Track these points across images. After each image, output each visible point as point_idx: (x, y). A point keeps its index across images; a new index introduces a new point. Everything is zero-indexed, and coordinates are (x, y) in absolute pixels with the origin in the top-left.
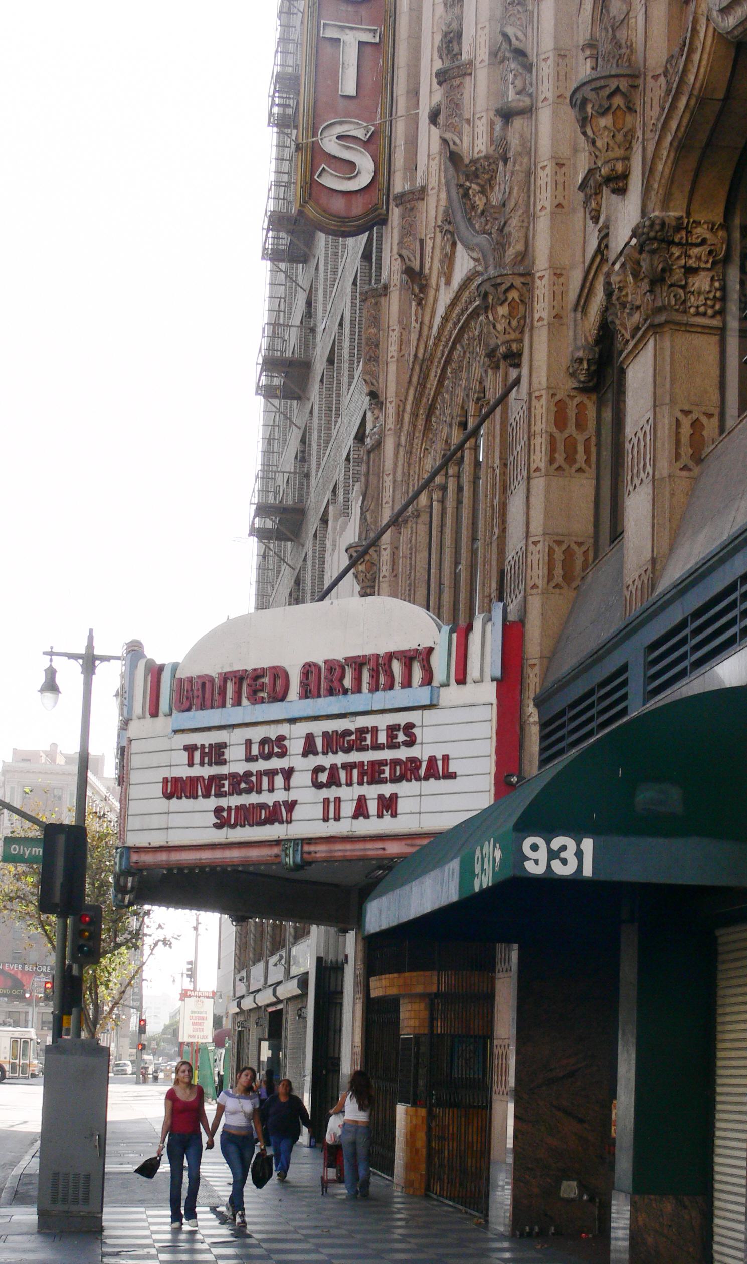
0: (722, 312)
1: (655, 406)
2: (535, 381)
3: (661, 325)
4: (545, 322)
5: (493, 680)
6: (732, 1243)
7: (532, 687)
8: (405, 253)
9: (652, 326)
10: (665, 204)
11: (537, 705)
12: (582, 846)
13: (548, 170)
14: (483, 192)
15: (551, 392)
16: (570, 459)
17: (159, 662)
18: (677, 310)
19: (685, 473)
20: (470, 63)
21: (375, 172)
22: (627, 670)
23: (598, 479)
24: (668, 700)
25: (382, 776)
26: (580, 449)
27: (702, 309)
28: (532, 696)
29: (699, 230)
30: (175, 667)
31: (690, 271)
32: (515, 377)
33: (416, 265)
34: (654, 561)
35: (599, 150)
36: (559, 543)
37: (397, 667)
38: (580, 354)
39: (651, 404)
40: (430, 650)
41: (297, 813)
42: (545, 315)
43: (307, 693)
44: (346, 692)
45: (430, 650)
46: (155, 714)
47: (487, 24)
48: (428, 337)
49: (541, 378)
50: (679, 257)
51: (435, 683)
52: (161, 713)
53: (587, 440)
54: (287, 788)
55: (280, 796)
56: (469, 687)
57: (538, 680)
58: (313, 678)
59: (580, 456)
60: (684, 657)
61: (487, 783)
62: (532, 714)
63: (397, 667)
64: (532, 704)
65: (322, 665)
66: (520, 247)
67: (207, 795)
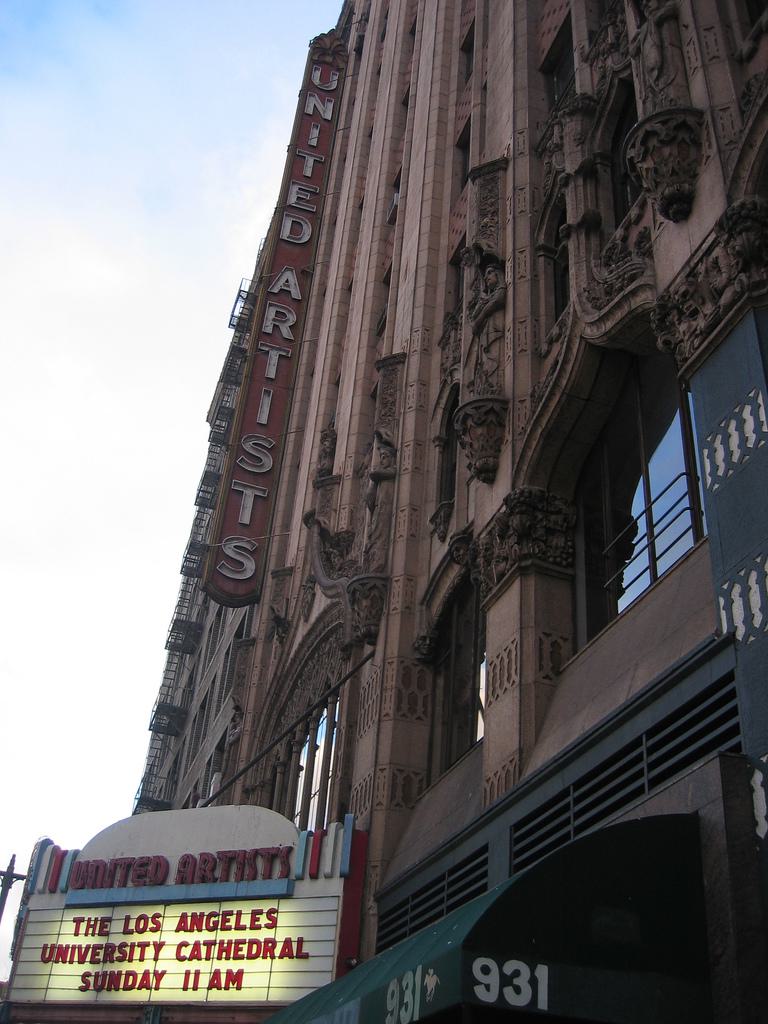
0: (572, 565)
1: (521, 628)
2: (389, 652)
3: (526, 568)
4: (399, 611)
5: (341, 876)
7: (373, 883)
8: (275, 607)
9: (519, 568)
10: (531, 480)
11: (377, 900)
12: (537, 974)
13: (406, 512)
14: (342, 556)
15: (402, 659)
16: (412, 709)
17: (63, 848)
18: (539, 558)
19: (546, 681)
20: (340, 477)
21: (256, 570)
22: (733, 679)
23: (432, 727)
24: (625, 819)
25: (240, 953)
26: (420, 702)
27: (558, 559)
28: (373, 892)
29: (557, 502)
30: (76, 853)
31: (550, 531)
32: (369, 652)
33: (283, 615)
34: (521, 750)
35: (476, 451)
37: (260, 864)
38: (423, 633)
39: (517, 626)
40: (290, 849)
41: (165, 982)
42: (399, 606)
43: (181, 880)
44: (215, 880)
45: (290, 849)
46: (53, 891)
47: (353, 455)
48: (286, 661)
49: (394, 649)
50: (541, 520)
51: (293, 877)
52: (59, 891)
53: (425, 697)
54: (156, 959)
55: (149, 965)
56: (321, 881)
57: (378, 878)
58: (189, 869)
59: (420, 708)
60: (441, 901)
61: (329, 964)
62: (372, 908)
63: (260, 864)
64: (372, 898)
66: (382, 562)
67: (82, 961)
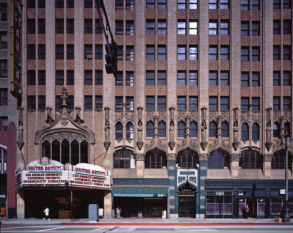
56: (65, 171)
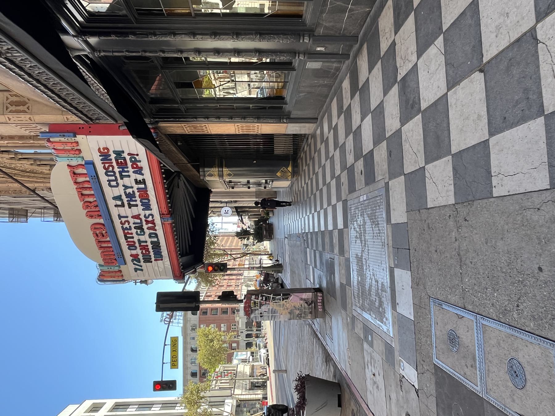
6: (300, 223)
36: (7, 108)
58: (92, 214)
65: (87, 210)
